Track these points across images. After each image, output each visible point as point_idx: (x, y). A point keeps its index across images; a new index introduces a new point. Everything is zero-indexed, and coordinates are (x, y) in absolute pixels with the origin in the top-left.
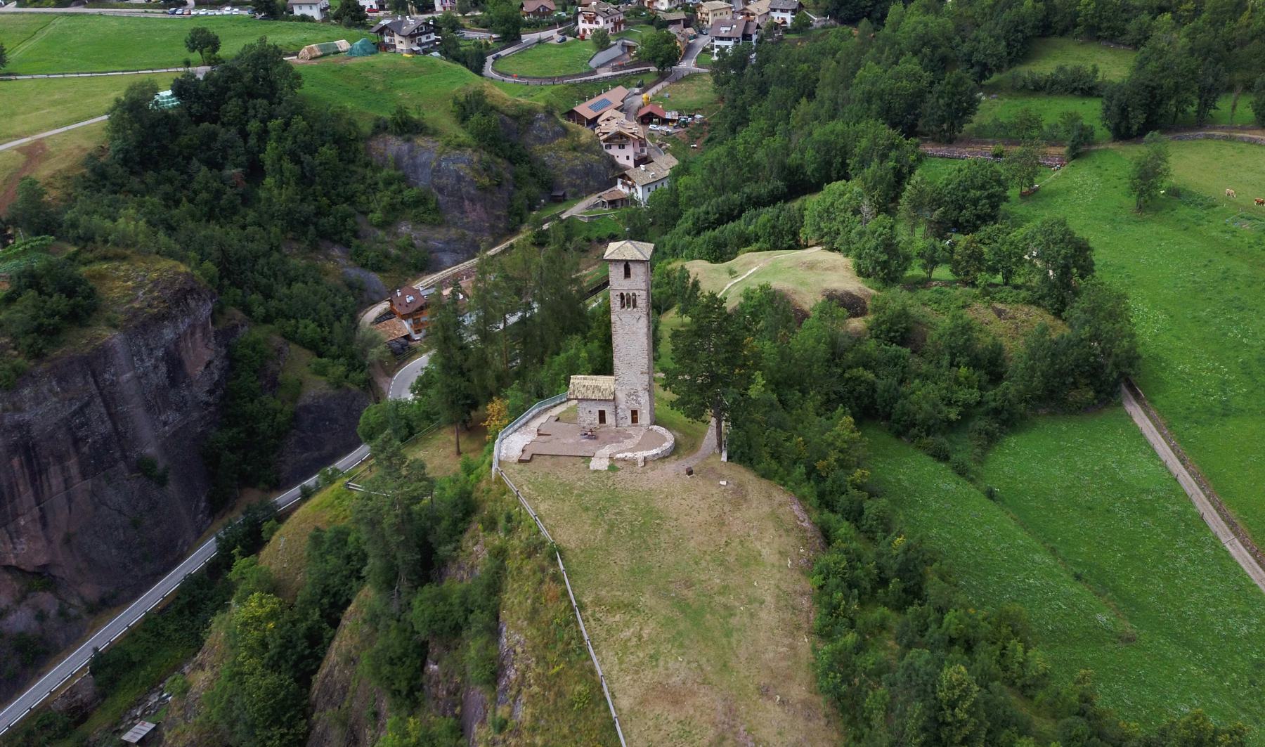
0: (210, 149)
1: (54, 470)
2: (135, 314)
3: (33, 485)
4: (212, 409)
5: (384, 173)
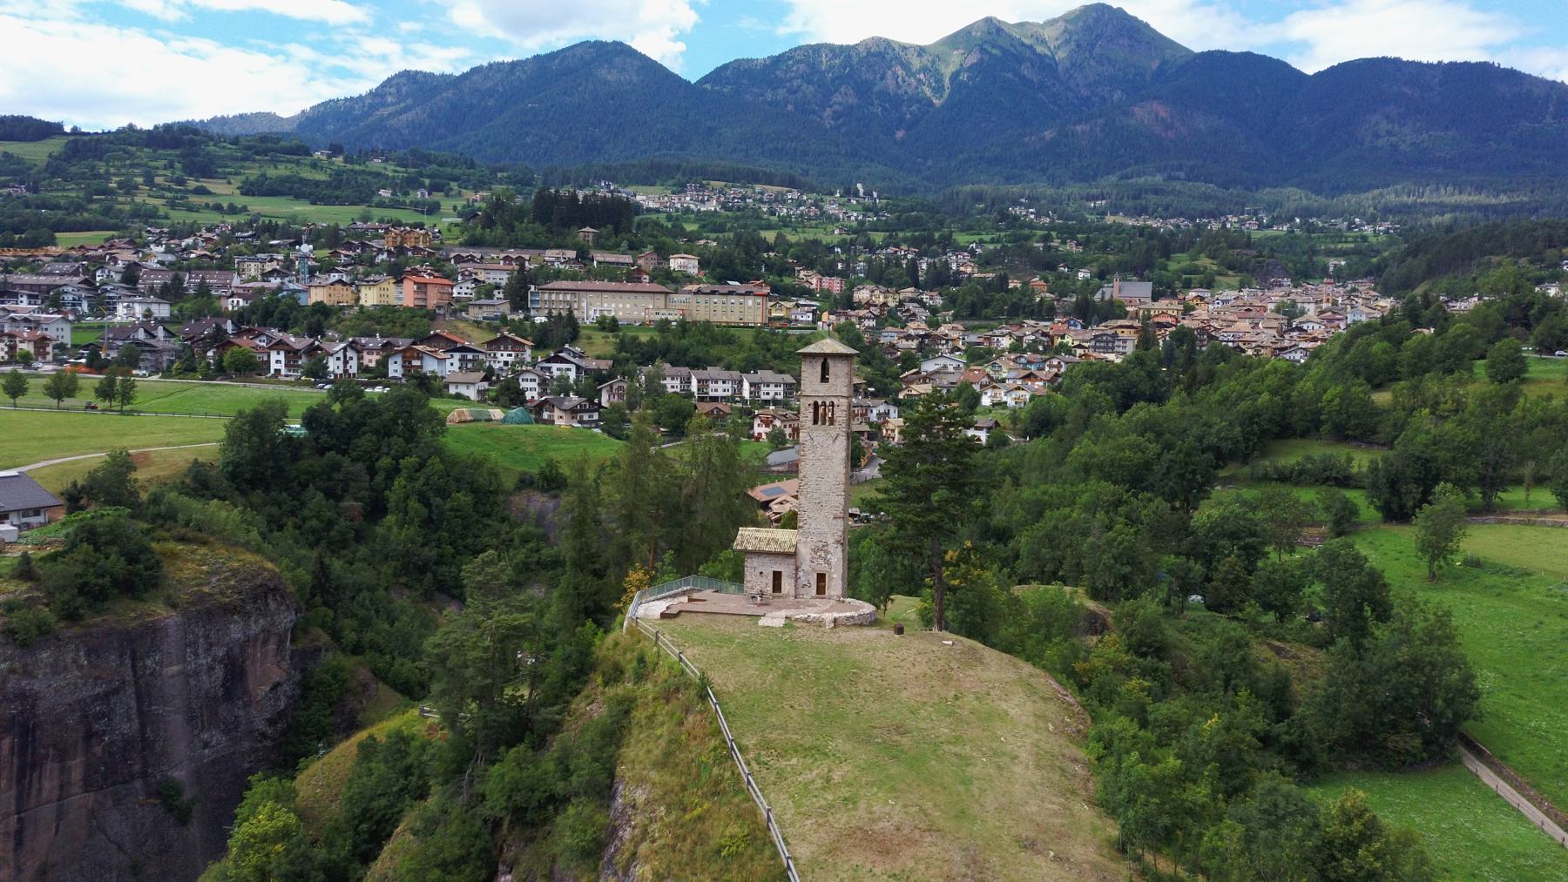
0: (330, 479)
1: (51, 768)
2: (202, 598)
3: (19, 782)
4: (268, 743)
5: (522, 529)
